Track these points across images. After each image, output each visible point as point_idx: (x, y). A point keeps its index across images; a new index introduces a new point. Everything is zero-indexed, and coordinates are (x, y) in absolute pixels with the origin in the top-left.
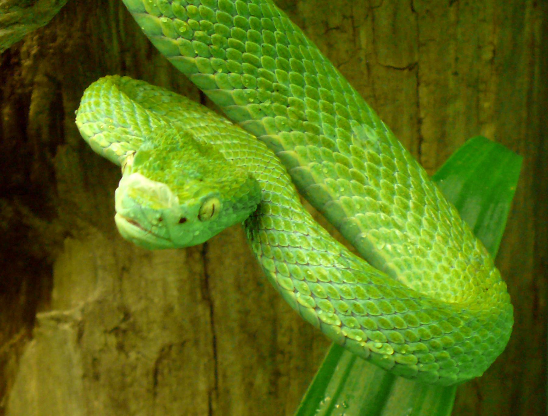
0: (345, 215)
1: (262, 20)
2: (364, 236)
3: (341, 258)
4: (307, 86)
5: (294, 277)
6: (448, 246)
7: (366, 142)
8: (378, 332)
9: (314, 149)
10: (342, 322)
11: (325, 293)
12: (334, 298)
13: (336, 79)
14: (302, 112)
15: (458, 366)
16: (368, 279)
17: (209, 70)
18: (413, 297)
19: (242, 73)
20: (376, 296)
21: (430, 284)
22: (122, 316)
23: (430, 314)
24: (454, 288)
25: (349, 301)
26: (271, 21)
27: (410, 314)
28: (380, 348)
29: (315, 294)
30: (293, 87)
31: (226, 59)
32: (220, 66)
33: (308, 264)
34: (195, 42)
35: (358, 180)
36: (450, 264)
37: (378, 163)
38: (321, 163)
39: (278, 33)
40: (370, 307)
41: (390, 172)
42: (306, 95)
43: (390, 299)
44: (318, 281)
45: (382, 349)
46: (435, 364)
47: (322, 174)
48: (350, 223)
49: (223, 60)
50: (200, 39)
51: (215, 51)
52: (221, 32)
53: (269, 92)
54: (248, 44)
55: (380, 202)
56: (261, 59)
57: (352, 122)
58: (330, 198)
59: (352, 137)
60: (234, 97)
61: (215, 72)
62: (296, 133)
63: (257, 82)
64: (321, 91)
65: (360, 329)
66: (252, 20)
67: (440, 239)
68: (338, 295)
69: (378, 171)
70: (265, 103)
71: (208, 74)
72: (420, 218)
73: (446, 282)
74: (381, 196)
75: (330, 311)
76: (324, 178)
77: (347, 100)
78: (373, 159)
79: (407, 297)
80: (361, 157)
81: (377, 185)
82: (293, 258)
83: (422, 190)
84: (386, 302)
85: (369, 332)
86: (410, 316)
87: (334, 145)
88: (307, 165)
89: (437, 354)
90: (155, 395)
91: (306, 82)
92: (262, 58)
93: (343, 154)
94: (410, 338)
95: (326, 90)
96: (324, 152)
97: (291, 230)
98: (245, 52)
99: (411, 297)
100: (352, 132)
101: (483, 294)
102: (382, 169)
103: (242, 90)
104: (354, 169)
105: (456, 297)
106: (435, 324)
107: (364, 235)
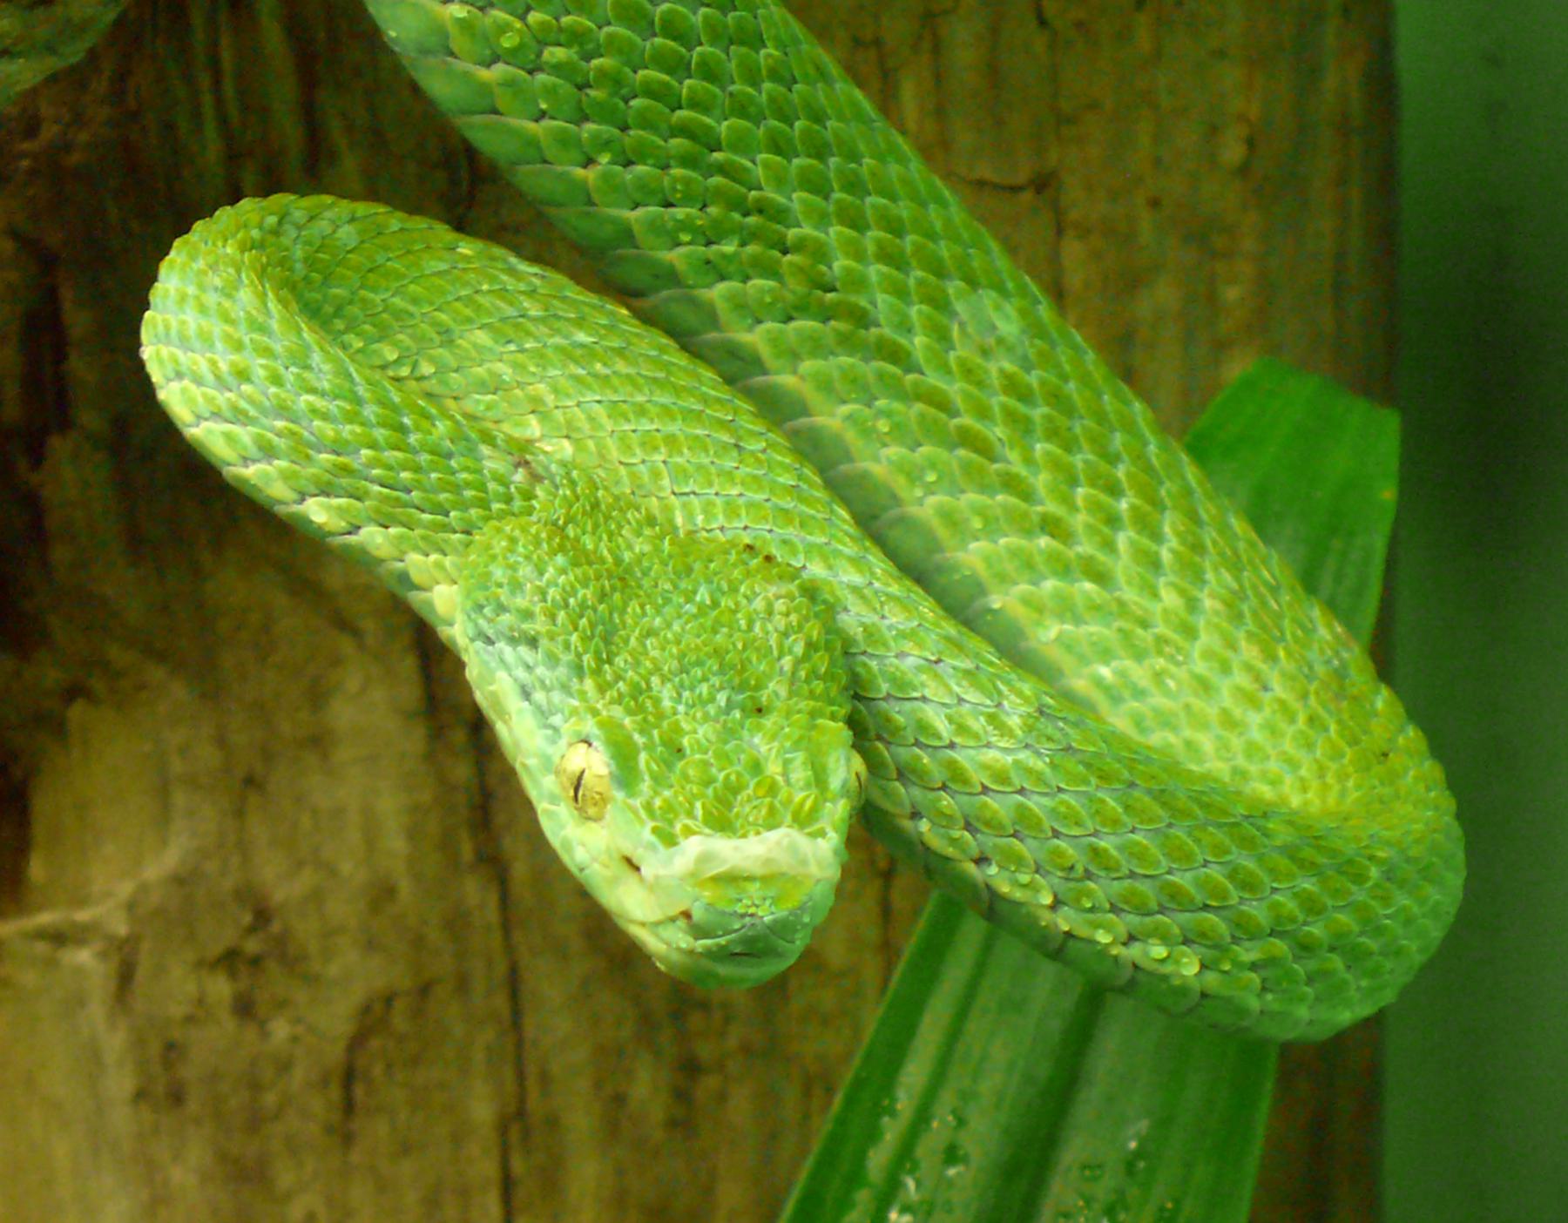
0: (935, 546)
2: (996, 606)
3: (1042, 720)
5: (908, 778)
6: (1245, 627)
7: (992, 341)
8: (1160, 917)
9: (852, 366)
10: (1055, 896)
11: (1007, 822)
12: (1033, 834)
13: (907, 168)
14: (823, 268)
15: (1359, 988)
16: (1126, 775)
18: (1246, 813)
20: (1151, 820)
21: (1206, 742)
22: (247, 918)
23: (1292, 858)
24: (1285, 753)
25: (1077, 841)
26: (753, 19)
27: (1245, 863)
28: (1163, 961)
29: (979, 825)
30: (803, 202)
31: (624, 128)
32: (606, 145)
33: (952, 746)
34: (541, 77)
35: (977, 451)
37: (1026, 396)
38: (869, 405)
39: (769, 55)
40: (1140, 855)
41: (1062, 421)
42: (834, 221)
43: (1188, 826)
44: (985, 790)
45: (1170, 961)
46: (1307, 989)
47: (874, 436)
48: (955, 568)
49: (616, 132)
50: (558, 69)
53: (736, 216)
54: (689, 87)
55: (1039, 509)
56: (724, 128)
57: (954, 287)
58: (896, 500)
60: (636, 228)
61: (589, 162)
63: (707, 189)
64: (873, 206)
65: (1110, 911)
66: (706, 18)
67: (1218, 605)
68: (1047, 824)
70: (725, 245)
71: (566, 168)
72: (1154, 547)
73: (1257, 735)
74: (1042, 491)
75: (1023, 869)
76: (879, 446)
77: (938, 226)
78: (1012, 386)
79: (1235, 816)
81: (1029, 461)
82: (905, 728)
83: (1149, 469)
84: (1179, 834)
85: (1133, 919)
86: (1244, 867)
87: (909, 354)
88: (833, 415)
89: (1313, 965)
90: (348, 1139)
91: (836, 186)
92: (726, 123)
93: (933, 379)
94: (1244, 930)
95: (884, 201)
96: (881, 376)
97: (888, 648)
98: (680, 107)
99: (1242, 815)
100: (953, 314)
101: (1377, 769)
102: (1039, 413)
103: (662, 209)
104: (967, 420)
105: (1302, 779)
106: (1309, 885)
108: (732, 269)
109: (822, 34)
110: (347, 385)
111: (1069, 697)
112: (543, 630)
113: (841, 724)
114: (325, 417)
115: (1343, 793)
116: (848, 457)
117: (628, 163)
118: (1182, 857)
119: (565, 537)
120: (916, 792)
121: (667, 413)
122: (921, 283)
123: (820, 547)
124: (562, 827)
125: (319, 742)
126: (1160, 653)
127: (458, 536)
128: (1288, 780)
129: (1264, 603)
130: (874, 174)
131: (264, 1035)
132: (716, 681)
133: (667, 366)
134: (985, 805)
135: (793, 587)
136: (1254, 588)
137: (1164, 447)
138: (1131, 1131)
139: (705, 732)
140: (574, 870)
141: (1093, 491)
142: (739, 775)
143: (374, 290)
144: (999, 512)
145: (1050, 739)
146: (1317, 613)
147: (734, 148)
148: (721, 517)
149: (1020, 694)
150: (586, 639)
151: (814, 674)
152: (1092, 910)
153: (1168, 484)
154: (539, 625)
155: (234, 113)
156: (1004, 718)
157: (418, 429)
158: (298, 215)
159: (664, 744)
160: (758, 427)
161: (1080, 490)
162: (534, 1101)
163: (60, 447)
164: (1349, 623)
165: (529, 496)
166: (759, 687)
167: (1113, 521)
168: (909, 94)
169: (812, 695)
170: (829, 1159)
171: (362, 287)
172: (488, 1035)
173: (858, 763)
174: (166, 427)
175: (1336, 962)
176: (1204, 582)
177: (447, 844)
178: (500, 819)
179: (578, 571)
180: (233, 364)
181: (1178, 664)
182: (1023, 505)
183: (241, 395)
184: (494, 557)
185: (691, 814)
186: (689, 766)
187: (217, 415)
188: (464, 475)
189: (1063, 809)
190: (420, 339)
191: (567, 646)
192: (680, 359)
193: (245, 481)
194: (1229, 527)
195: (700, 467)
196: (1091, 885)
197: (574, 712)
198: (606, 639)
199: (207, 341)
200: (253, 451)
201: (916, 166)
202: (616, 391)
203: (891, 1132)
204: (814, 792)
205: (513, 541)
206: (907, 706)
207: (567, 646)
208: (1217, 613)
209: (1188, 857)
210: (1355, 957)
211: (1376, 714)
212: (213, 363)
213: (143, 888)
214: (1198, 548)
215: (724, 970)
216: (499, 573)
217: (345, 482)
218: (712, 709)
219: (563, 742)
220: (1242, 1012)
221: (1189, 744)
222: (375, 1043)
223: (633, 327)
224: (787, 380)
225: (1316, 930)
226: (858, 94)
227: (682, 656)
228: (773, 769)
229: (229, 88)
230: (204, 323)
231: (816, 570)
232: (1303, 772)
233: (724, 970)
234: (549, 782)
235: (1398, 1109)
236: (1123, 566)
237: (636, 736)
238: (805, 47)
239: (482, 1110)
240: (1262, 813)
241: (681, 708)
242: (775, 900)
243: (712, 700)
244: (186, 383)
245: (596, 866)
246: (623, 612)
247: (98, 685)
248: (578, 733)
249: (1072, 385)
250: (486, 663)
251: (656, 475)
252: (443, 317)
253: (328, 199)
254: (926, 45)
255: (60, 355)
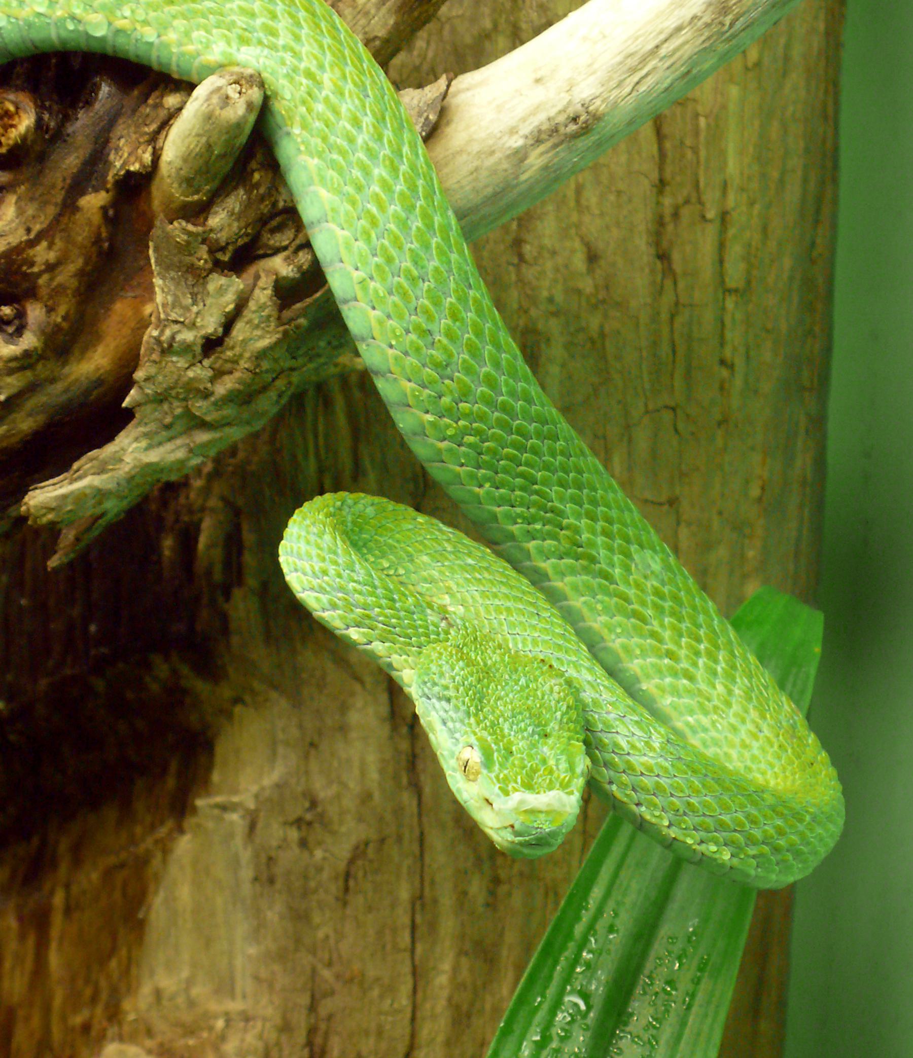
0: (619, 661)
1: (546, 427)
2: (644, 688)
4: (586, 506)
7: (649, 573)
17: (475, 482)
19: (513, 491)
20: (714, 792)
21: (734, 754)
22: (307, 805)
23: (773, 811)
28: (714, 852)
30: (571, 508)
31: (497, 473)
32: (488, 479)
33: (628, 754)
34: (463, 448)
35: (639, 619)
36: (757, 727)
37: (661, 597)
40: (705, 805)
41: (677, 608)
44: (642, 774)
48: (626, 670)
50: (470, 446)
51: (486, 462)
52: (496, 440)
53: (542, 513)
54: (526, 457)
57: (634, 548)
59: (633, 566)
61: (481, 486)
62: (568, 561)
64: (602, 511)
66: (535, 428)
67: (742, 694)
68: (668, 791)
69: (663, 608)
73: (756, 752)
77: (629, 521)
78: (657, 593)
80: (643, 591)
81: (662, 625)
83: (714, 632)
85: (703, 834)
87: (612, 576)
88: (577, 601)
89: (779, 857)
90: (345, 904)
93: (622, 588)
94: (751, 841)
96: (600, 585)
98: (521, 465)
100: (632, 559)
101: (809, 770)
102: (668, 605)
104: (636, 606)
106: (779, 822)
107: (644, 686)
108: (538, 535)
109: (581, 432)
110: (370, 579)
111: (676, 731)
112: (453, 695)
113: (581, 744)
114: (360, 593)
115: (794, 781)
116: (583, 620)
117: (497, 488)
118: (726, 808)
119: (463, 653)
120: (612, 773)
121: (506, 596)
122: (620, 545)
123: (573, 662)
124: (457, 782)
125: (343, 729)
126: (715, 713)
127: (415, 649)
128: (769, 773)
129: (761, 693)
130: (602, 498)
131: (311, 854)
132: (528, 721)
133: (507, 576)
134: (642, 781)
135: (562, 681)
136: (758, 686)
137: (721, 622)
138: (690, 924)
139: (522, 744)
140: (462, 802)
141: (689, 640)
142: (537, 765)
143: (381, 536)
144: (648, 647)
145: (671, 753)
146: (784, 699)
147: (543, 484)
148: (530, 646)
149: (659, 733)
150: (472, 700)
151: (570, 720)
152: (685, 829)
153: (722, 638)
154: (451, 693)
155: (322, 452)
156: (652, 743)
157: (400, 600)
158: (350, 502)
159: (504, 749)
160: (547, 606)
161: (683, 639)
162: (427, 890)
163: (237, 593)
164: (797, 702)
165: (447, 633)
166: (546, 725)
167: (697, 654)
168: (617, 460)
169: (569, 730)
170: (556, 928)
171: (376, 534)
172: (408, 862)
173: (588, 761)
174: (286, 588)
175: (790, 857)
176: (736, 682)
177: (396, 778)
178: (420, 766)
179: (469, 669)
180: (320, 568)
181: (723, 718)
182: (659, 645)
183: (323, 581)
184: (432, 661)
185: (516, 782)
186: (515, 760)
187: (312, 589)
188: (420, 622)
189: (675, 785)
190: (399, 558)
191: (464, 703)
192: (513, 573)
193: (323, 619)
194: (748, 659)
195: (521, 623)
196: (686, 818)
197: (466, 733)
198: (480, 699)
199: (310, 558)
200: (327, 606)
201: (620, 495)
202: (484, 586)
203: (586, 917)
204: (569, 774)
205: (441, 654)
206: (610, 735)
207: (464, 703)
208: (741, 697)
209: (729, 808)
210: (797, 854)
211: (808, 745)
212: (312, 566)
213: (263, 789)
214: (733, 667)
215: (526, 851)
216: (434, 668)
217: (367, 622)
218: (525, 734)
219: (460, 745)
220: (747, 875)
221: (726, 754)
222: (360, 863)
223: (492, 558)
224: (558, 584)
225: (782, 842)
226: (597, 462)
227: (513, 710)
228: (552, 762)
229: (321, 440)
230: (308, 548)
231: (572, 673)
232: (776, 769)
233: (526, 851)
234: (453, 762)
235: (800, 914)
236: (700, 674)
237: (493, 745)
238: (576, 441)
239: (404, 894)
240: (761, 790)
241: (513, 733)
242: (551, 822)
243: (526, 730)
244: (299, 574)
245: (472, 801)
246: (488, 688)
247: (247, 698)
248: (467, 742)
249: (682, 593)
250: (427, 708)
251: (501, 624)
252: (409, 549)
253: (362, 495)
254: (626, 439)
255: (240, 553)
